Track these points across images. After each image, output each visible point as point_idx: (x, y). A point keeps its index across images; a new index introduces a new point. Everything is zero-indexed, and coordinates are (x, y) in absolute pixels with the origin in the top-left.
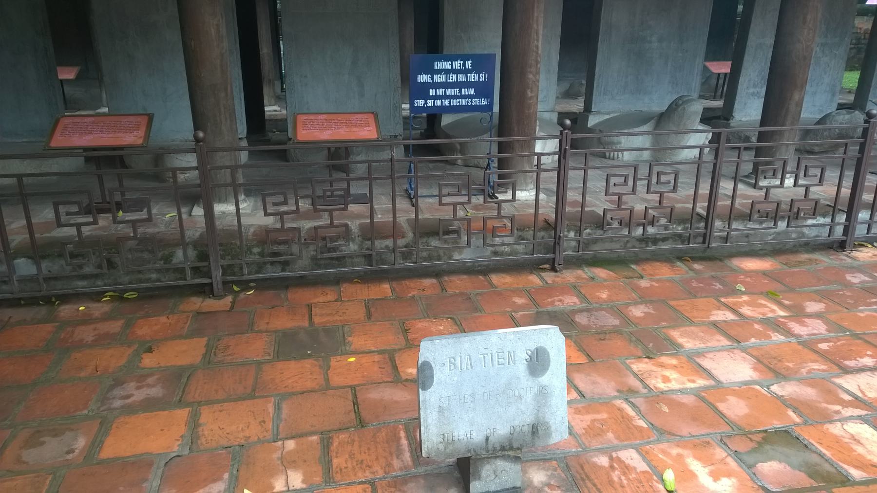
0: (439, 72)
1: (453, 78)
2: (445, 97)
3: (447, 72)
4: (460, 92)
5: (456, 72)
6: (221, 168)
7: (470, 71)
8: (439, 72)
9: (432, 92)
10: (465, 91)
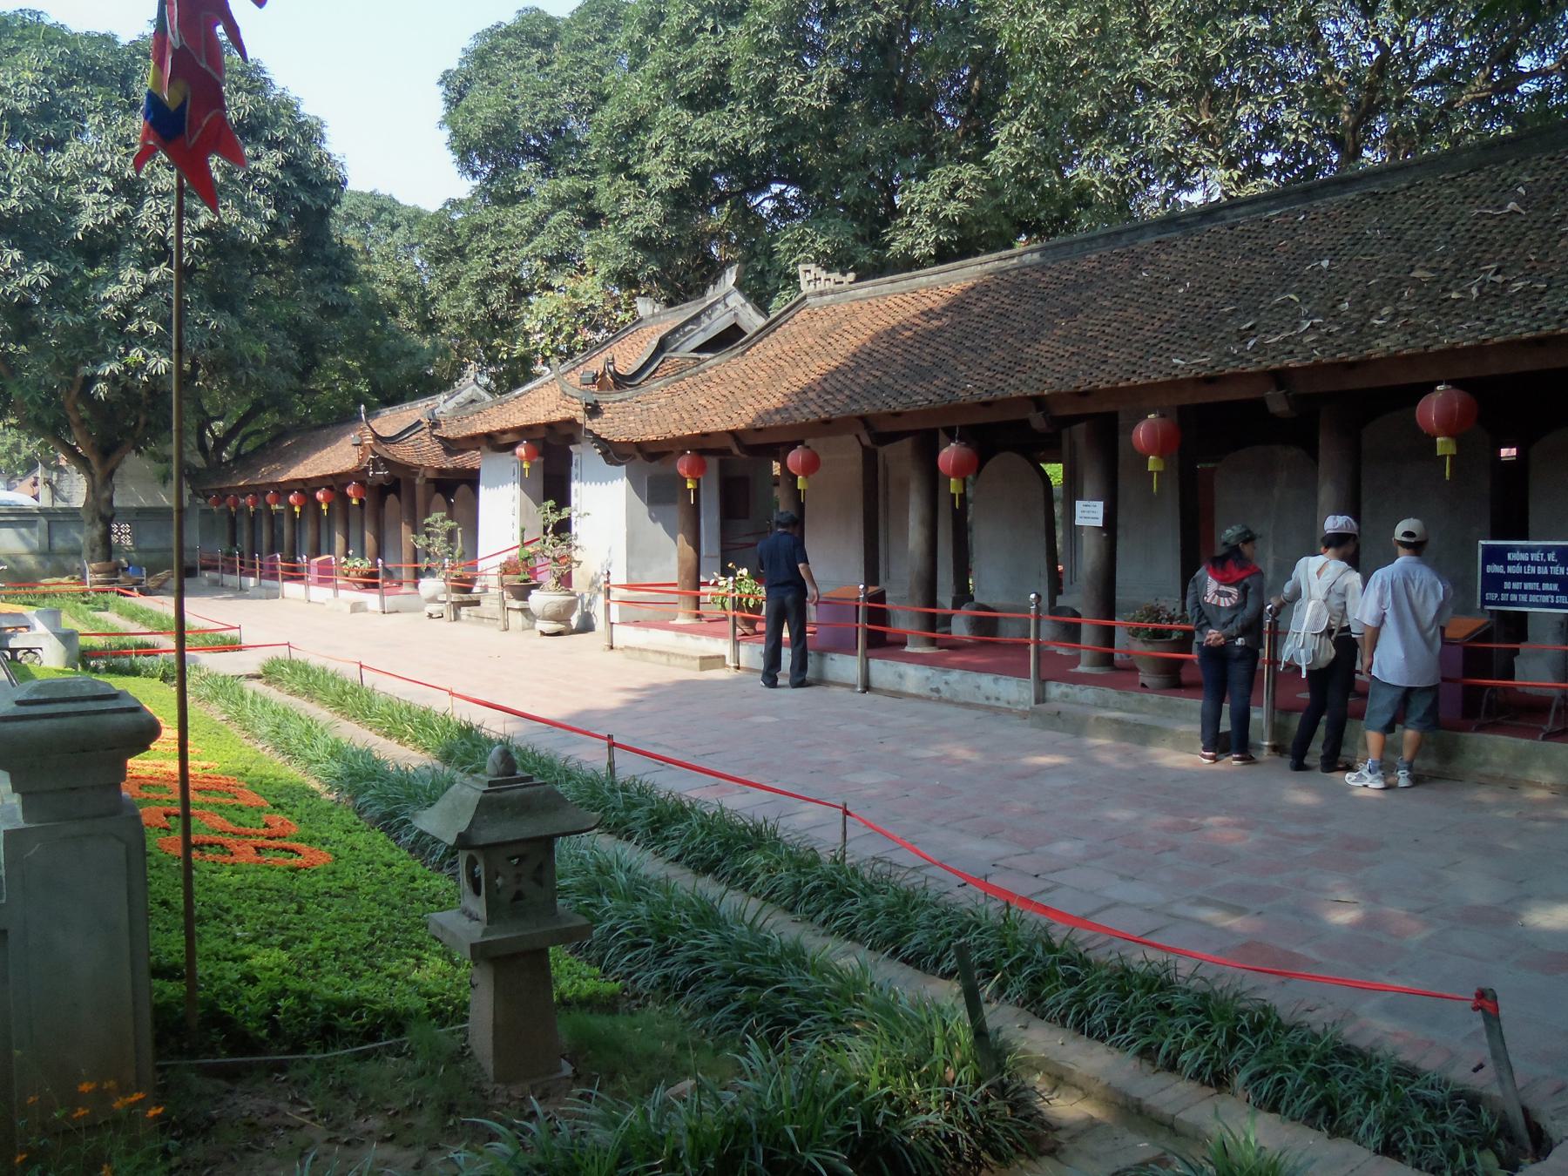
0: (1514, 563)
1: (1531, 570)
2: (1522, 591)
3: (1524, 563)
4: (1540, 586)
5: (1535, 564)
6: (611, 765)
7: (1554, 564)
8: (1514, 563)
9: (1507, 585)
10: (1546, 586)
